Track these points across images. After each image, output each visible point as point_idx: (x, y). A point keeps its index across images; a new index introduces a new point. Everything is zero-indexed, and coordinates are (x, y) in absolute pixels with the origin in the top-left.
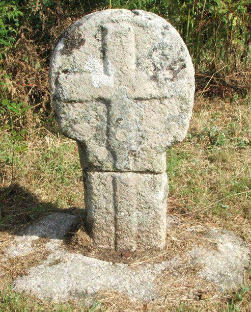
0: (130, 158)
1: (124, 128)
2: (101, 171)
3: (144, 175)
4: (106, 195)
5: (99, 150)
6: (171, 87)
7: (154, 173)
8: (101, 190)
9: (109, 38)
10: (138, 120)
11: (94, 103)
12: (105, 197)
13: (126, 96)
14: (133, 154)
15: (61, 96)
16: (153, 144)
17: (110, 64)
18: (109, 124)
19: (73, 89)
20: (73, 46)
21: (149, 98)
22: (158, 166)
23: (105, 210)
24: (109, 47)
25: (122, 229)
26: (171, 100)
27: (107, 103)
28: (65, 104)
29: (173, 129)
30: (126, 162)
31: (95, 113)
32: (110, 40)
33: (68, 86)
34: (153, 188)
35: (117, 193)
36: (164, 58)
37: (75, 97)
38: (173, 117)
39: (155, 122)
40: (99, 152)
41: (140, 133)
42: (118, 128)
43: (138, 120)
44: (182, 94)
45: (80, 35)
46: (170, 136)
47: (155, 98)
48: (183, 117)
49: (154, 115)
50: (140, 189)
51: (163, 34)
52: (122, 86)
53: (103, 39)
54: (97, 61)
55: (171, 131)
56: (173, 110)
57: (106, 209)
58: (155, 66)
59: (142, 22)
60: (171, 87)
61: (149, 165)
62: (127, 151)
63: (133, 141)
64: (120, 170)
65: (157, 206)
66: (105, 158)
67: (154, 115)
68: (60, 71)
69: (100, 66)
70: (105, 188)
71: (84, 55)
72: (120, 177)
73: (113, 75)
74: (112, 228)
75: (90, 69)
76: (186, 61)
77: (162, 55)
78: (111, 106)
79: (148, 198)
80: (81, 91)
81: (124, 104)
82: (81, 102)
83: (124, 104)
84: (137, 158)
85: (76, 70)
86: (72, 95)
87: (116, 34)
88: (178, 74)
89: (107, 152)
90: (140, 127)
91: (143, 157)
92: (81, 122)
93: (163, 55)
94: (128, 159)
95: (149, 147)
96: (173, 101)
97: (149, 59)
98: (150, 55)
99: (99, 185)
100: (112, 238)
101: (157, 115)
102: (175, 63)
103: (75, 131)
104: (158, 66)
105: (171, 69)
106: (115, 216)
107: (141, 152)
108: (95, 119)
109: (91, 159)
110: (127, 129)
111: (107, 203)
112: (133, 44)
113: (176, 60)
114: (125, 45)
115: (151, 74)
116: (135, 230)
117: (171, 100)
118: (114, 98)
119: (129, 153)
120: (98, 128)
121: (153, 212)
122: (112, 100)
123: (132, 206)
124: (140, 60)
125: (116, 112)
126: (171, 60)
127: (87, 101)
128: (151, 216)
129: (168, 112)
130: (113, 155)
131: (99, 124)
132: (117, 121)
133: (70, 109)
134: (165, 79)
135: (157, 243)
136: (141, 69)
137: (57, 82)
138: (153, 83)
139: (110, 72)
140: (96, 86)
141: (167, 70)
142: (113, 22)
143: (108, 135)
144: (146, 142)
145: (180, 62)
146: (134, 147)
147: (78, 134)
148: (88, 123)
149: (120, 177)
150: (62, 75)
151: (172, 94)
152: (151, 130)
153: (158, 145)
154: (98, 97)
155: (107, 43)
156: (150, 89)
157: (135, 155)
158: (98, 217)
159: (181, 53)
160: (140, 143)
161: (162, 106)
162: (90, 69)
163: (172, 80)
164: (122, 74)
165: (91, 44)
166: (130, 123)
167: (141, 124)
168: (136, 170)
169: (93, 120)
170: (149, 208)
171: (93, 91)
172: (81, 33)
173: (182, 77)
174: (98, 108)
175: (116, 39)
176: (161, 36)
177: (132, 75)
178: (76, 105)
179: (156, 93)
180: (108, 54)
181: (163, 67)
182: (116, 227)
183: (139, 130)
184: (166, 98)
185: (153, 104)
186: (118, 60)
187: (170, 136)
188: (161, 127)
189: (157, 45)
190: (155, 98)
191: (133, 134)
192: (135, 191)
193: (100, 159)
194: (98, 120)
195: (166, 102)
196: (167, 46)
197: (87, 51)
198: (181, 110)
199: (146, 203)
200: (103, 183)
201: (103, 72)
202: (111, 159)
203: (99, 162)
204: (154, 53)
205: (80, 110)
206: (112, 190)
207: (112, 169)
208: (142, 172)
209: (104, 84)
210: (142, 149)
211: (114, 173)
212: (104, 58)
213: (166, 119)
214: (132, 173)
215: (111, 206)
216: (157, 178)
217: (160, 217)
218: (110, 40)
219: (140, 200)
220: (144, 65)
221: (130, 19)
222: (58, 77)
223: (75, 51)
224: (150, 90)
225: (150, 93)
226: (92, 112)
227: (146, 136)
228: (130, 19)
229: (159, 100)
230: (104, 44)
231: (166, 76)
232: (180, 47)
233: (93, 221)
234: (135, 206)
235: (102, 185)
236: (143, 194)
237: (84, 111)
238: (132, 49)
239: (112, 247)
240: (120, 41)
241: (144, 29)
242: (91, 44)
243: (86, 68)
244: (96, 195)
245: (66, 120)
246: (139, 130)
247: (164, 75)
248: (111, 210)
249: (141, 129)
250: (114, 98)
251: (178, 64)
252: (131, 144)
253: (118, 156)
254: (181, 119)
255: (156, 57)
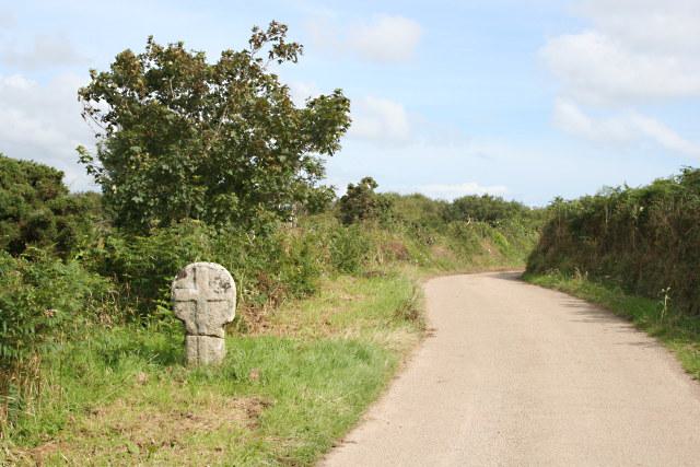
9: (197, 273)
14: (208, 327)
27: (196, 302)
33: (178, 294)
40: (191, 325)
69: (192, 284)
125: (199, 307)
130: (198, 326)
156: (214, 296)
164: (203, 289)
179: (217, 298)
210: (57, 212)
233: (585, 202)
242: (190, 275)
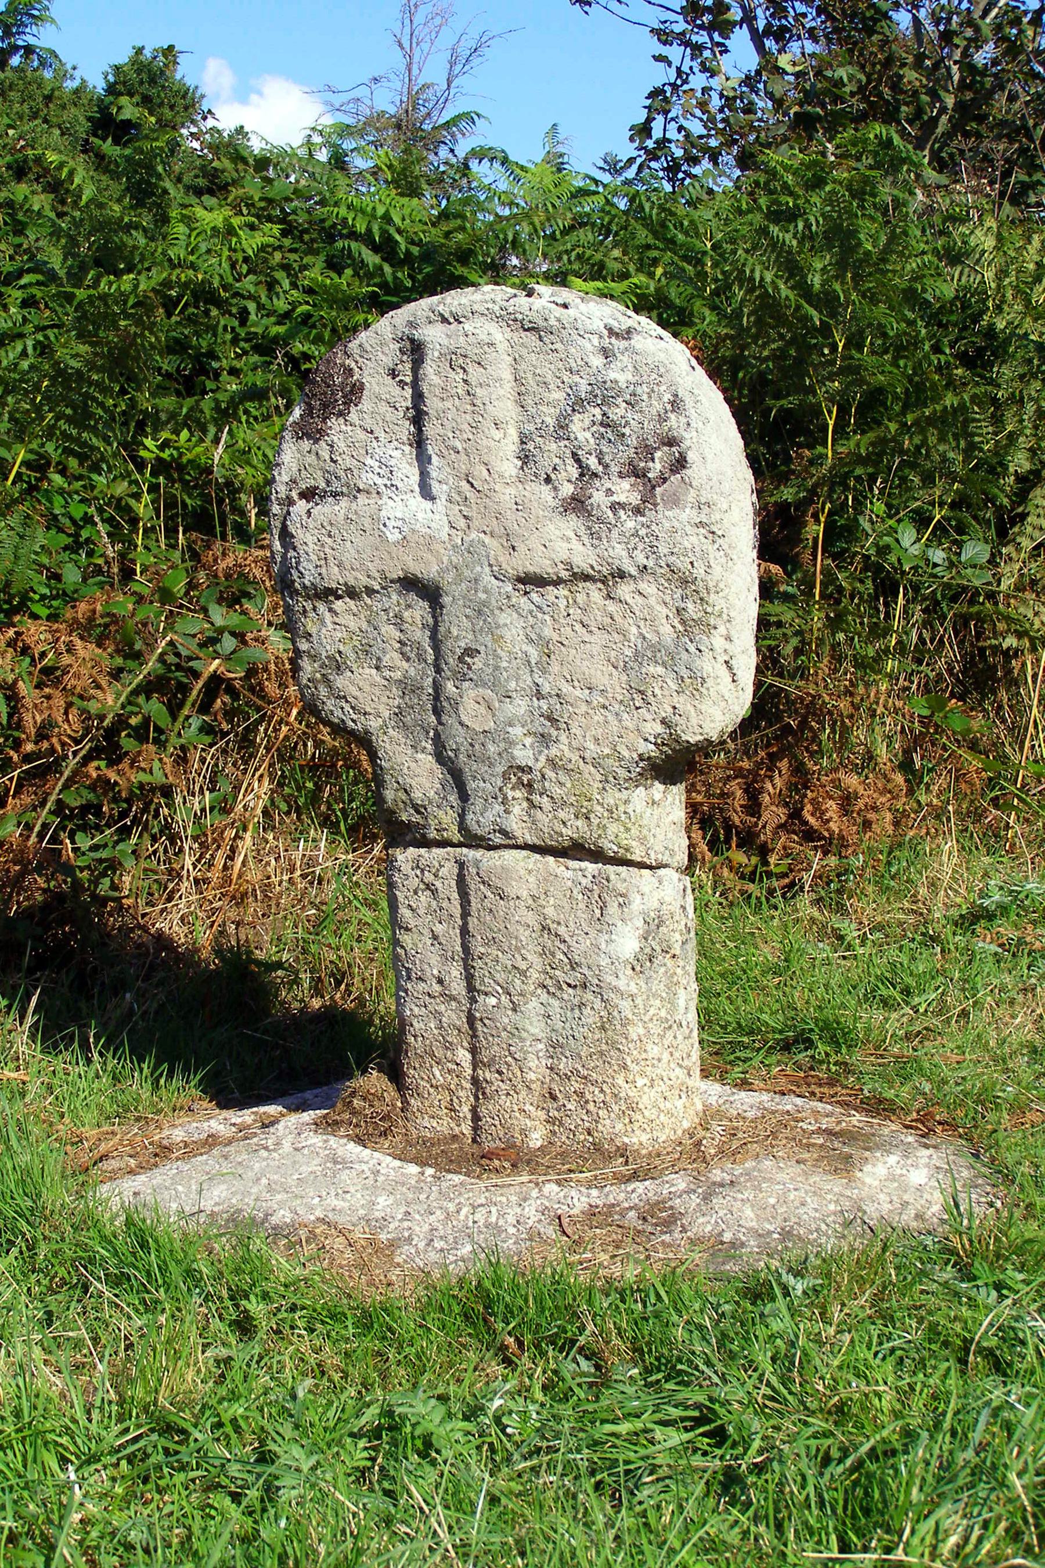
0: (510, 794)
1: (484, 685)
2: (426, 843)
3: (571, 863)
4: (439, 929)
5: (413, 765)
6: (636, 534)
7: (597, 855)
8: (421, 912)
10: (534, 654)
11: (395, 597)
12: (435, 937)
13: (487, 569)
15: (295, 575)
16: (590, 745)
17: (435, 459)
18: (438, 670)
19: (327, 550)
20: (328, 409)
21: (565, 575)
22: (613, 828)
23: (437, 988)
24: (432, 404)
25: (493, 1060)
26: (643, 586)
27: (428, 592)
28: (309, 606)
29: (657, 691)
30: (498, 808)
31: (398, 634)
32: (436, 380)
34: (598, 912)
35: (473, 923)
36: (610, 435)
37: (334, 577)
38: (655, 648)
39: (591, 665)
41: (544, 704)
42: (466, 684)
43: (534, 654)
44: (681, 563)
45: (349, 372)
46: (648, 717)
47: (587, 578)
48: (692, 648)
49: (587, 637)
50: (550, 911)
51: (606, 353)
52: (473, 535)
53: (415, 384)
54: (397, 454)
55: (651, 699)
56: (651, 621)
57: (440, 981)
58: (578, 461)
59: (533, 316)
60: (636, 534)
61: (579, 823)
62: (500, 769)
63: (517, 731)
64: (482, 838)
65: (609, 978)
66: (431, 794)
67: (587, 637)
68: (294, 494)
70: (434, 903)
71: (362, 435)
72: (477, 863)
73: (444, 497)
74: (464, 1056)
75: (379, 481)
76: (688, 443)
77: (601, 424)
78: (442, 607)
79: (580, 947)
80: (349, 554)
81: (484, 596)
82: (352, 593)
83: (484, 596)
84: (536, 798)
85: (336, 486)
86: (324, 571)
87: (455, 360)
88: (658, 490)
89: (438, 771)
90: (540, 681)
91: (557, 791)
92: (354, 667)
93: (606, 423)
94: (505, 797)
95: (575, 757)
96: (649, 587)
97: (559, 438)
98: (562, 426)
99: (416, 893)
100: (465, 1094)
101: (599, 638)
102: (648, 452)
103: (339, 697)
104: (592, 462)
105: (636, 472)
106: (470, 1011)
107: (550, 774)
108: (397, 656)
109: (389, 795)
110: (494, 686)
111: (445, 959)
112: (507, 388)
113: (651, 442)
114: (479, 392)
115: (567, 490)
116: (536, 1068)
117: (643, 586)
118: (450, 577)
119: (505, 777)
120: (408, 687)
121: (598, 1004)
122: (444, 584)
123: (523, 973)
124: (530, 446)
125: (459, 631)
126: (633, 441)
127: (370, 592)
128: (590, 1017)
129: (634, 630)
131: (412, 672)
132: (461, 659)
133: (323, 622)
134: (615, 507)
135: (619, 1126)
136: (536, 475)
137: (285, 535)
138: (573, 523)
139: (436, 488)
140: (393, 536)
141: (621, 475)
142: (445, 320)
143: (437, 712)
144: (563, 738)
145: (666, 448)
146: (523, 755)
147: (347, 707)
148: (378, 668)
149: (477, 863)
150: (301, 506)
151: (641, 560)
152: (578, 693)
153: (607, 751)
154: (401, 574)
155: (425, 389)
156: (562, 542)
157: (530, 785)
158: (416, 1010)
159: (672, 416)
160: (544, 739)
161: (612, 607)
162: (379, 481)
163: (638, 511)
165: (382, 396)
166: (505, 664)
167: (544, 671)
168: (538, 842)
169: (391, 657)
170: (584, 986)
171: (386, 556)
172: (353, 365)
173: (675, 501)
174: (406, 614)
175: (452, 374)
176: (597, 361)
177: (507, 495)
178: (338, 605)
179: (584, 557)
180: (430, 430)
181: (606, 466)
182: (474, 1051)
183: (539, 695)
184: (621, 575)
185: (581, 598)
186: (459, 446)
187: (648, 717)
188: (614, 683)
189: (584, 388)
190: (587, 578)
191: (520, 707)
192: (531, 918)
193: (417, 795)
194: (408, 660)
195: (624, 590)
196: (620, 393)
197: (369, 423)
198: (683, 622)
199: (574, 965)
200: (428, 887)
201: (417, 489)
202: (453, 798)
203: (417, 808)
204: (577, 417)
205: (353, 624)
206: (457, 912)
207: (457, 837)
208: (559, 852)
209: (417, 527)
211: (465, 850)
212: (419, 442)
213: (628, 652)
214: (525, 853)
215: (455, 973)
216: (612, 877)
217: (625, 1023)
218: (436, 380)
219: (553, 954)
220: (545, 464)
221: (497, 308)
222: (289, 513)
223: (335, 424)
224: (565, 545)
225: (564, 555)
226: (390, 631)
227: (563, 713)
228: (497, 308)
229: (600, 585)
230: (418, 397)
231: (615, 498)
232: (667, 397)
234: (534, 975)
235: (428, 893)
236: (562, 930)
237: (364, 626)
238: (505, 408)
239: (466, 1129)
240: (465, 381)
241: (541, 339)
242: (382, 396)
243: (366, 479)
244: (407, 929)
245: (314, 658)
246: (539, 695)
247: (609, 492)
248: (458, 987)
249: (546, 689)
250: (450, 577)
251: (658, 455)
252: (512, 743)
253: (471, 785)
254: (684, 655)
255: (581, 429)
